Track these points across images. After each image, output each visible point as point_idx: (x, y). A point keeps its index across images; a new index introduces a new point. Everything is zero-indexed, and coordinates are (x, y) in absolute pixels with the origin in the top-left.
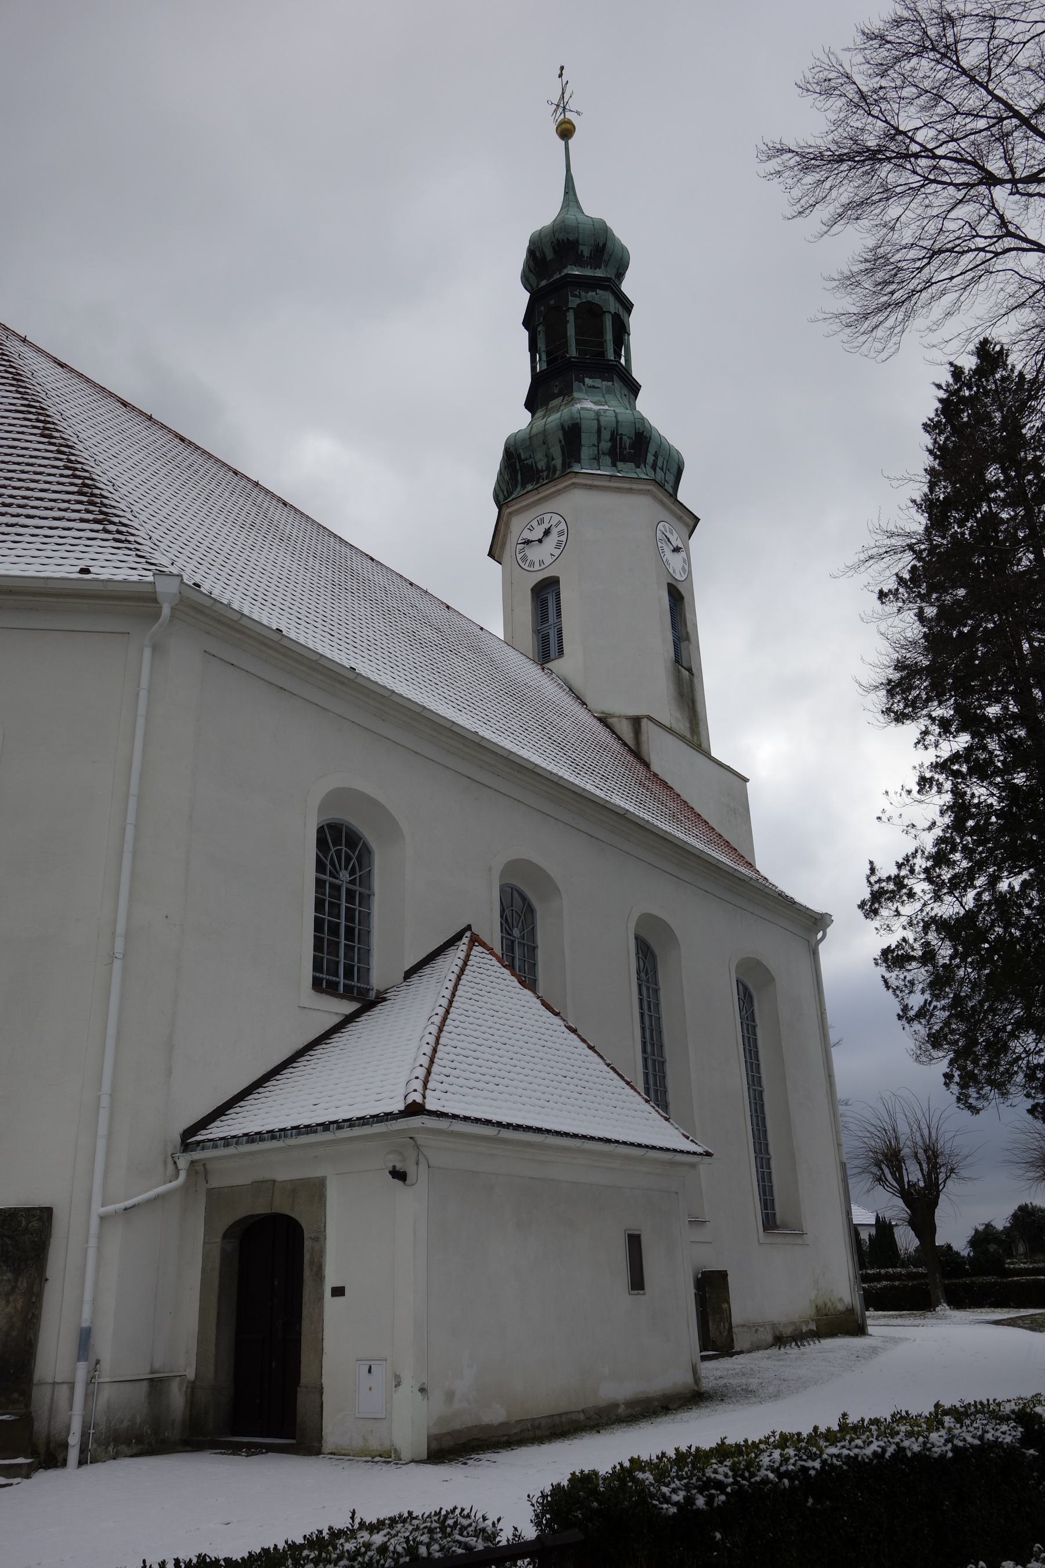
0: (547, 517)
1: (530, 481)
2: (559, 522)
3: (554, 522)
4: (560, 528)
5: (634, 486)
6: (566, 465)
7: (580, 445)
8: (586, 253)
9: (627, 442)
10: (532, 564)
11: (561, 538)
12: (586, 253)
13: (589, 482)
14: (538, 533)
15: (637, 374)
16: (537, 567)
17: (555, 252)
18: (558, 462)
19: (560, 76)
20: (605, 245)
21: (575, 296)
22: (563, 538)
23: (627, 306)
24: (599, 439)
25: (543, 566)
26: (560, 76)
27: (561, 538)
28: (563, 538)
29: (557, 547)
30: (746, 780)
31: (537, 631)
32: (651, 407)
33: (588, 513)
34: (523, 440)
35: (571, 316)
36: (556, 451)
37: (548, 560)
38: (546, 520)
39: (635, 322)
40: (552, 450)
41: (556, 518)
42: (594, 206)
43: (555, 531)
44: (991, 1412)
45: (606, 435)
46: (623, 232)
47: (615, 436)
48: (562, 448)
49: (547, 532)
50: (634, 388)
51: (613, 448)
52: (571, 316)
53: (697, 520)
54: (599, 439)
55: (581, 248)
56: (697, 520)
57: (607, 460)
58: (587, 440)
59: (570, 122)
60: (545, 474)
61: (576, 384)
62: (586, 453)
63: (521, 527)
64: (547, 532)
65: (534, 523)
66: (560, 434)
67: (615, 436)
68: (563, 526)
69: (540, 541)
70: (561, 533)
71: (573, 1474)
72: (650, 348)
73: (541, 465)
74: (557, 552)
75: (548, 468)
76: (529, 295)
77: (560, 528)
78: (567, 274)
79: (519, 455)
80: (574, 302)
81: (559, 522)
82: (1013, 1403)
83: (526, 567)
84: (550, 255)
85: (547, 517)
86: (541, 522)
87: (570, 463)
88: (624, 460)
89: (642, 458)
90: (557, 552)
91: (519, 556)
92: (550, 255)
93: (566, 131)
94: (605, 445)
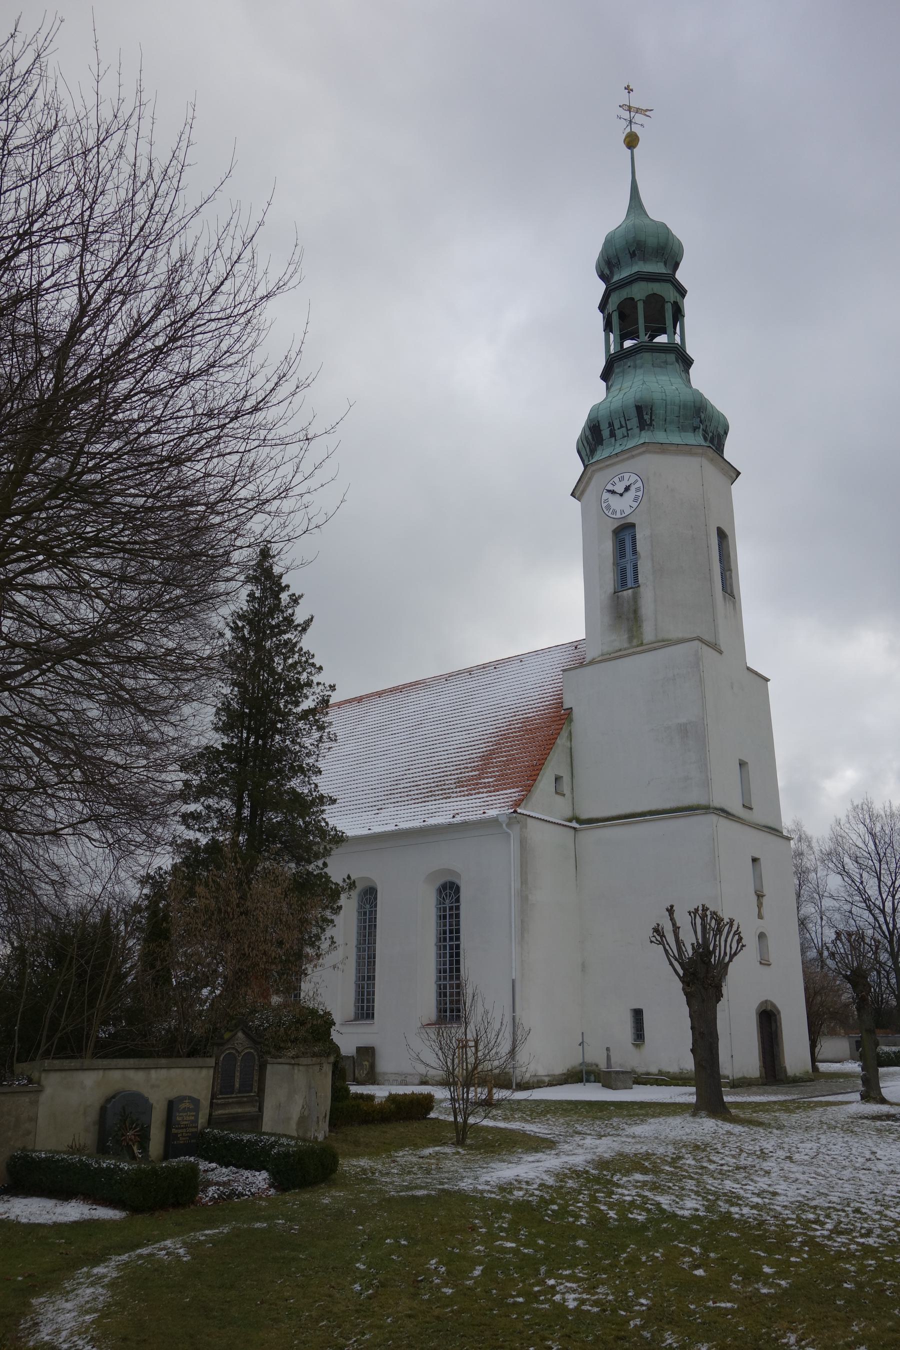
0: (626, 476)
2: (636, 481)
3: (631, 481)
4: (637, 485)
10: (614, 512)
11: (638, 494)
14: (620, 488)
15: (690, 351)
16: (618, 515)
20: (667, 239)
23: (682, 292)
25: (623, 515)
27: (638, 494)
28: (640, 494)
29: (635, 500)
30: (767, 680)
31: (616, 564)
32: (705, 379)
33: (661, 474)
38: (626, 478)
39: (688, 304)
42: (657, 210)
43: (633, 488)
46: (677, 230)
49: (627, 489)
50: (686, 362)
53: (738, 474)
56: (738, 474)
63: (599, 480)
64: (627, 489)
65: (616, 480)
69: (621, 495)
70: (638, 490)
74: (635, 505)
76: (605, 286)
77: (637, 485)
81: (636, 481)
82: (881, 1146)
83: (609, 514)
85: (626, 476)
86: (621, 479)
89: (705, 429)
90: (635, 505)
91: (604, 505)
93: (632, 141)
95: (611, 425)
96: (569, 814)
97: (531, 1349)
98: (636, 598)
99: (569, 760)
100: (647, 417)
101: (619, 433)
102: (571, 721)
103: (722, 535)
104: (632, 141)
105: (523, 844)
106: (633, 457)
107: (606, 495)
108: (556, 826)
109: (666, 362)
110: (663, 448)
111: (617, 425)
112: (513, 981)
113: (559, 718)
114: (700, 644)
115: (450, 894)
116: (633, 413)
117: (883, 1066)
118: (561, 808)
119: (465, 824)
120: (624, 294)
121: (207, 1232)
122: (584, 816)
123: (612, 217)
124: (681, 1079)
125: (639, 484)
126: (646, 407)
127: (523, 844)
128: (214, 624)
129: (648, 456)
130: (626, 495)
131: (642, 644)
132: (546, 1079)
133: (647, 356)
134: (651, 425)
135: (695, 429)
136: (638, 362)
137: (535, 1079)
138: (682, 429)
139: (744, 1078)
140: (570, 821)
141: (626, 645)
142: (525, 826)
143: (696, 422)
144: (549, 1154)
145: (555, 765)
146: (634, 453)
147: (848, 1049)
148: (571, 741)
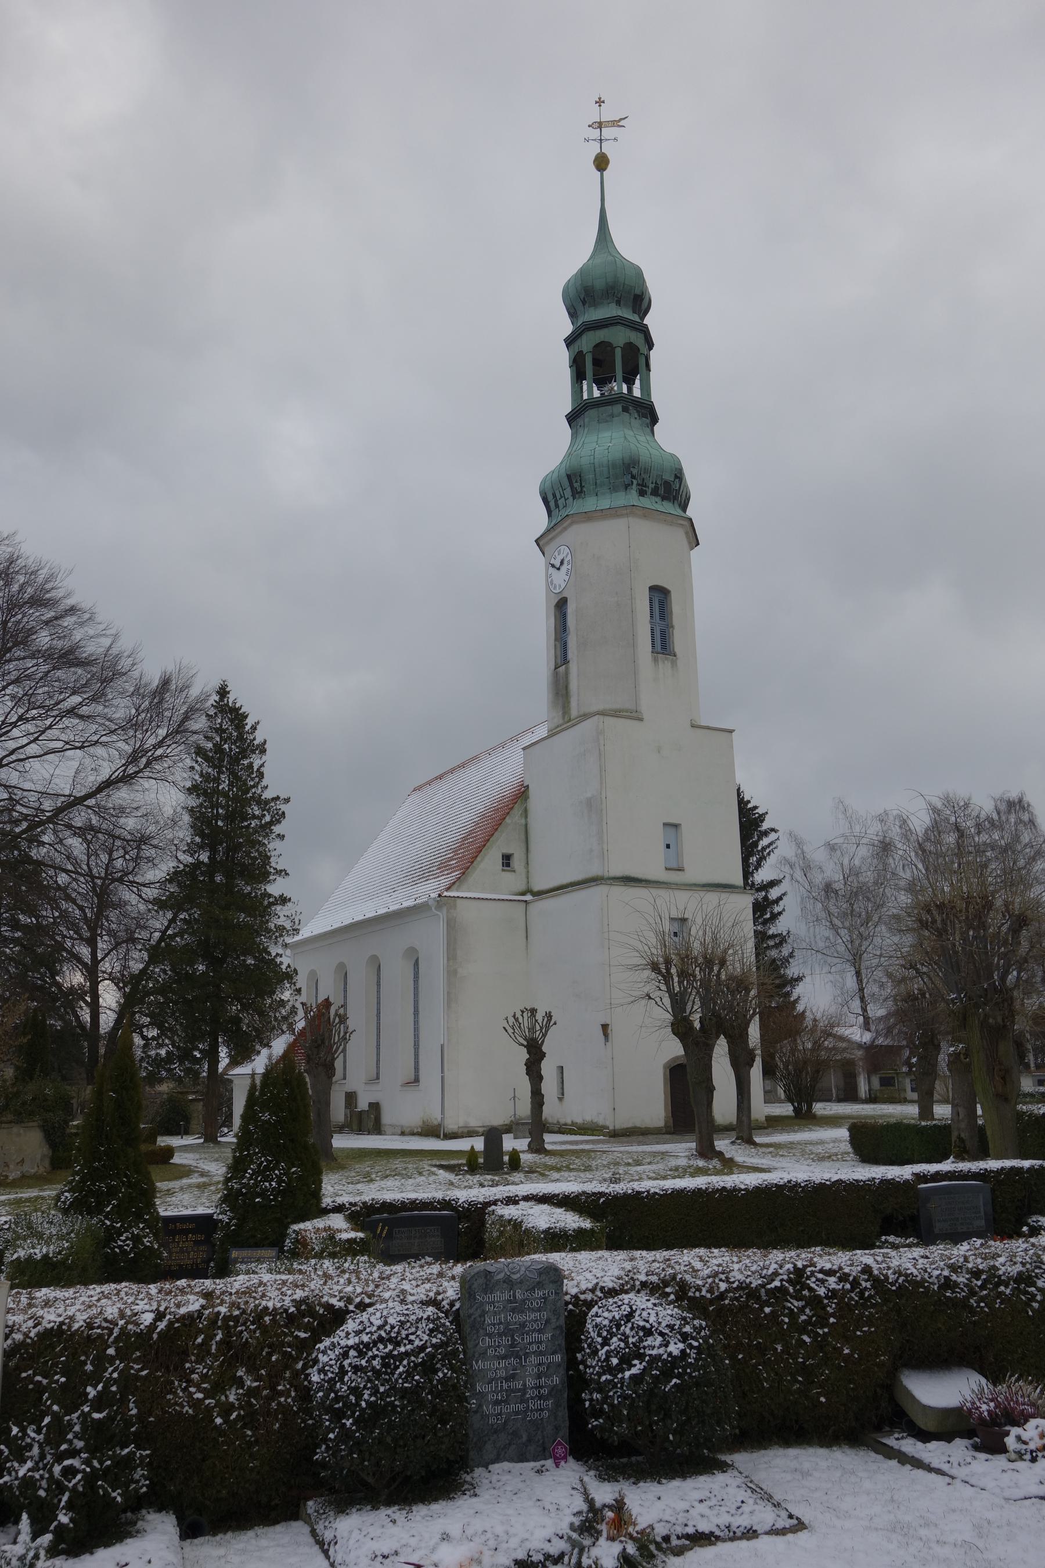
49: (562, 563)
93: (601, 163)
95: (554, 495)
96: (522, 887)
98: (567, 673)
99: (523, 836)
100: (577, 485)
101: (561, 502)
102: (527, 798)
103: (660, 596)
104: (601, 163)
105: (451, 926)
106: (565, 529)
108: (499, 903)
109: (612, 416)
110: (588, 517)
111: (558, 497)
112: (442, 1046)
113: (522, 794)
114: (601, 717)
116: (566, 483)
117: (163, 1134)
118: (513, 881)
119: (409, 909)
120: (601, 335)
122: (536, 889)
123: (575, 255)
124: (584, 1129)
126: (575, 475)
127: (451, 926)
129: (575, 528)
131: (570, 720)
132: (481, 1130)
133: (592, 413)
134: (581, 492)
135: (627, 487)
136: (586, 420)
137: (466, 1130)
138: (614, 489)
139: (635, 1127)
140: (523, 894)
141: (561, 722)
142: (455, 907)
143: (627, 479)
145: (505, 842)
146: (565, 525)
147: (529, 1106)
148: (526, 817)
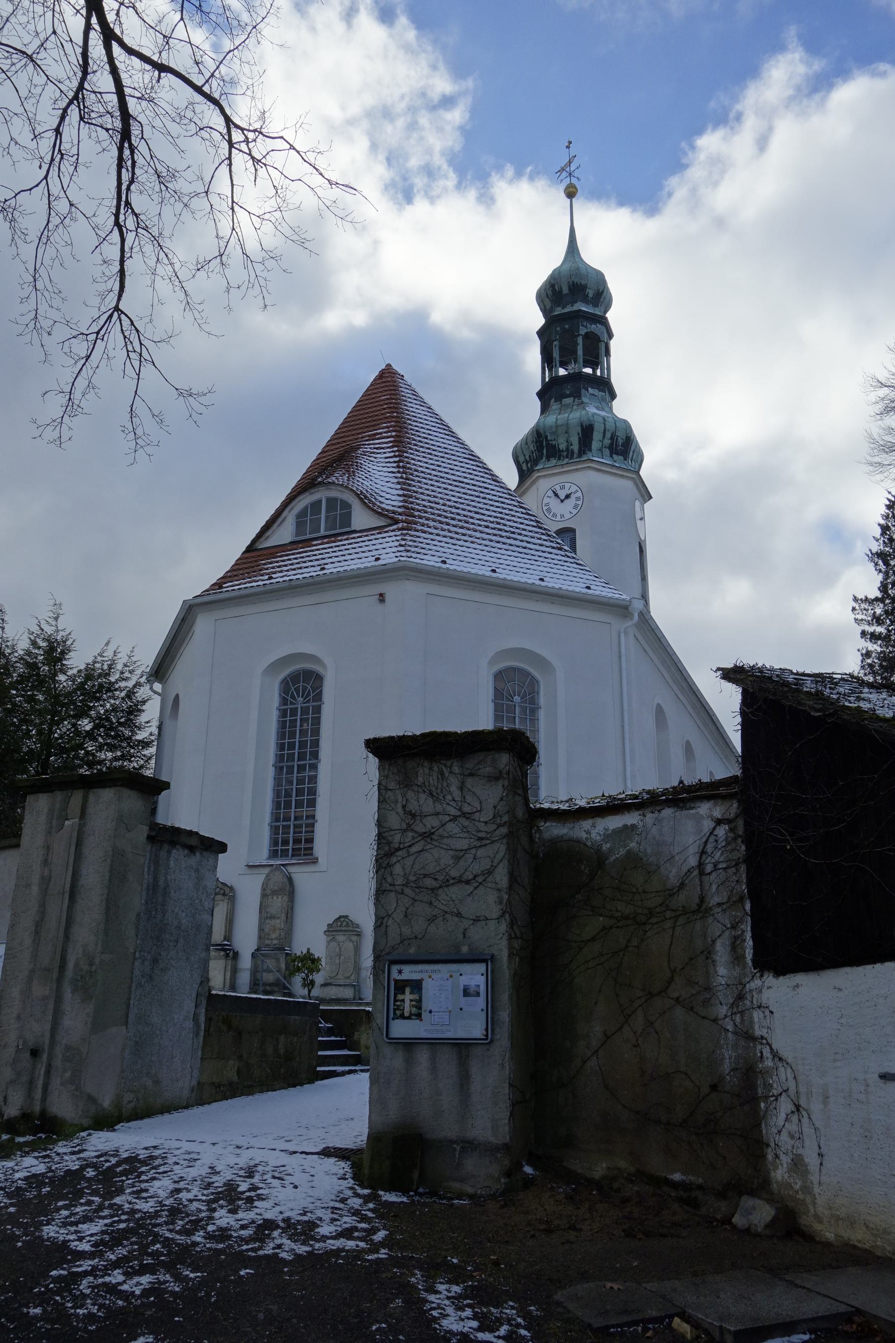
0: (567, 485)
1: (555, 457)
2: (577, 491)
5: (625, 474)
6: (581, 453)
7: (591, 439)
8: (591, 295)
9: (620, 441)
10: (555, 515)
12: (591, 295)
13: (599, 467)
16: (558, 518)
17: (570, 289)
18: (575, 447)
19: (568, 147)
20: (603, 291)
21: (583, 326)
22: (580, 503)
24: (604, 437)
26: (568, 147)
28: (580, 503)
29: (575, 507)
34: (551, 427)
35: (580, 340)
36: (575, 440)
37: (568, 516)
40: (571, 439)
41: (574, 488)
42: (593, 255)
43: (573, 497)
44: (846, 674)
45: (608, 435)
47: (613, 437)
48: (579, 438)
49: (568, 496)
51: (612, 444)
52: (580, 340)
53: (650, 497)
54: (604, 437)
55: (588, 290)
57: (607, 452)
58: (597, 436)
59: (575, 187)
60: (565, 453)
61: (583, 391)
62: (595, 445)
64: (568, 496)
66: (579, 429)
67: (613, 437)
68: (579, 494)
70: (578, 499)
71: (879, 589)
72: (624, 362)
73: (563, 446)
75: (567, 450)
78: (580, 311)
79: (546, 437)
80: (583, 331)
81: (577, 491)
84: (565, 290)
87: (584, 451)
88: (617, 454)
90: (575, 512)
91: (545, 508)
92: (565, 290)
94: (607, 442)
97: (892, 563)
107: (550, 493)
115: (304, 689)
121: (62, 1272)
123: (548, 261)
125: (579, 494)
128: (275, 898)
130: (566, 501)
144: (402, 97)
